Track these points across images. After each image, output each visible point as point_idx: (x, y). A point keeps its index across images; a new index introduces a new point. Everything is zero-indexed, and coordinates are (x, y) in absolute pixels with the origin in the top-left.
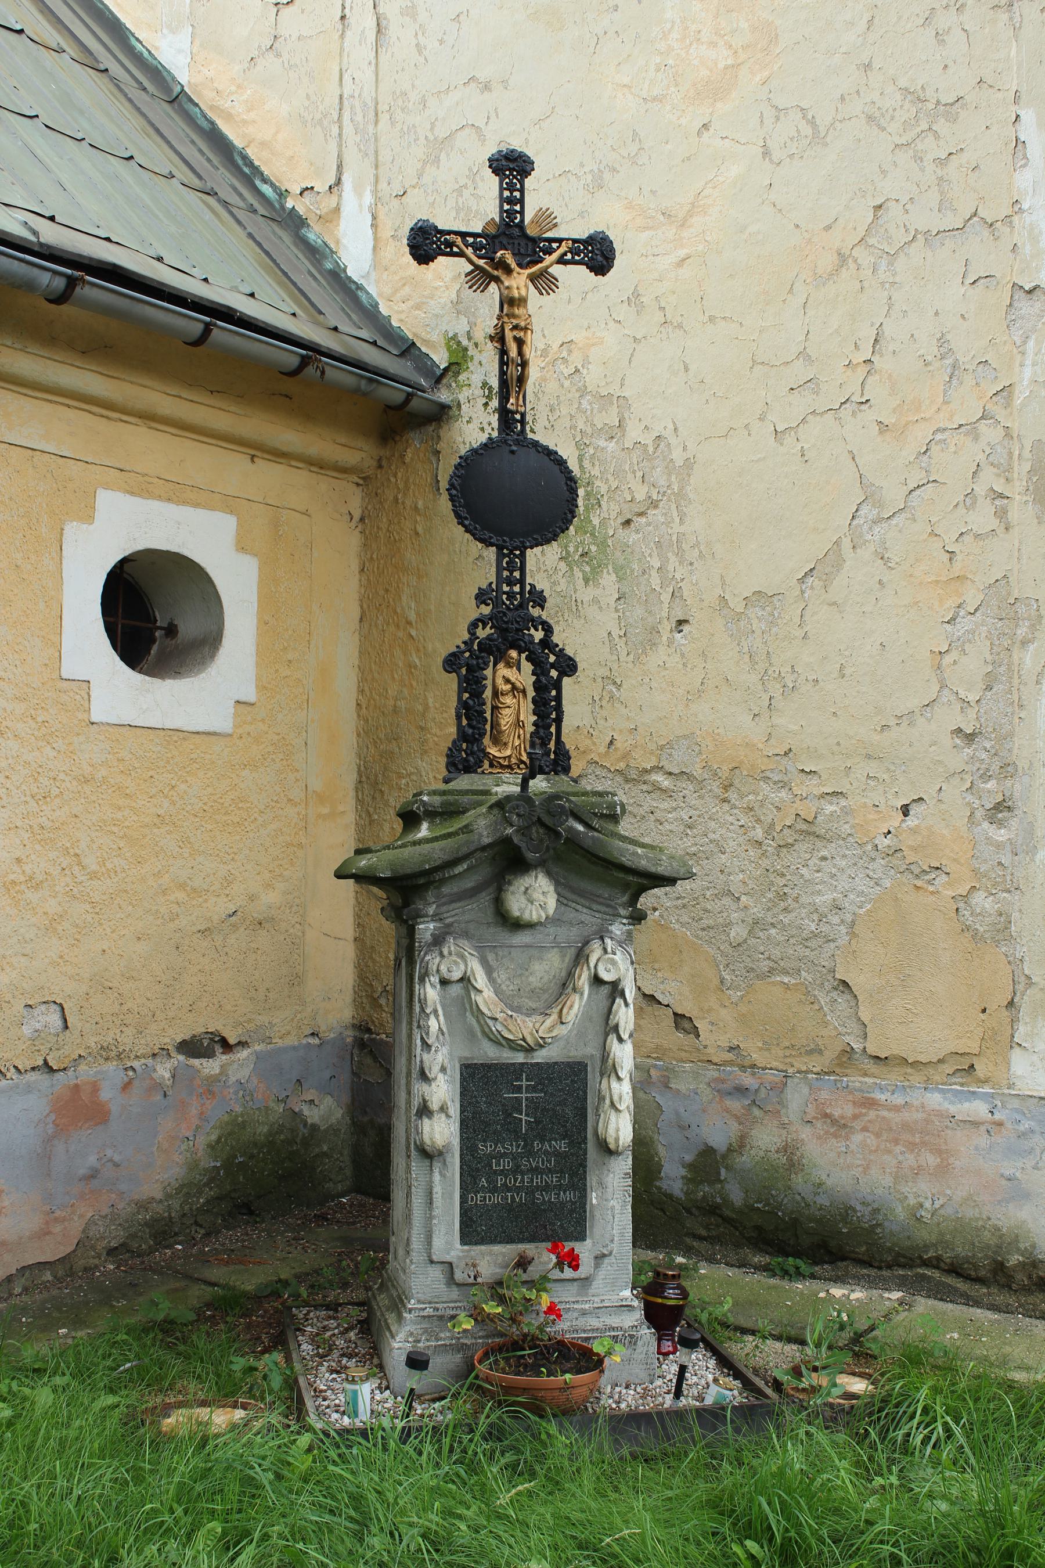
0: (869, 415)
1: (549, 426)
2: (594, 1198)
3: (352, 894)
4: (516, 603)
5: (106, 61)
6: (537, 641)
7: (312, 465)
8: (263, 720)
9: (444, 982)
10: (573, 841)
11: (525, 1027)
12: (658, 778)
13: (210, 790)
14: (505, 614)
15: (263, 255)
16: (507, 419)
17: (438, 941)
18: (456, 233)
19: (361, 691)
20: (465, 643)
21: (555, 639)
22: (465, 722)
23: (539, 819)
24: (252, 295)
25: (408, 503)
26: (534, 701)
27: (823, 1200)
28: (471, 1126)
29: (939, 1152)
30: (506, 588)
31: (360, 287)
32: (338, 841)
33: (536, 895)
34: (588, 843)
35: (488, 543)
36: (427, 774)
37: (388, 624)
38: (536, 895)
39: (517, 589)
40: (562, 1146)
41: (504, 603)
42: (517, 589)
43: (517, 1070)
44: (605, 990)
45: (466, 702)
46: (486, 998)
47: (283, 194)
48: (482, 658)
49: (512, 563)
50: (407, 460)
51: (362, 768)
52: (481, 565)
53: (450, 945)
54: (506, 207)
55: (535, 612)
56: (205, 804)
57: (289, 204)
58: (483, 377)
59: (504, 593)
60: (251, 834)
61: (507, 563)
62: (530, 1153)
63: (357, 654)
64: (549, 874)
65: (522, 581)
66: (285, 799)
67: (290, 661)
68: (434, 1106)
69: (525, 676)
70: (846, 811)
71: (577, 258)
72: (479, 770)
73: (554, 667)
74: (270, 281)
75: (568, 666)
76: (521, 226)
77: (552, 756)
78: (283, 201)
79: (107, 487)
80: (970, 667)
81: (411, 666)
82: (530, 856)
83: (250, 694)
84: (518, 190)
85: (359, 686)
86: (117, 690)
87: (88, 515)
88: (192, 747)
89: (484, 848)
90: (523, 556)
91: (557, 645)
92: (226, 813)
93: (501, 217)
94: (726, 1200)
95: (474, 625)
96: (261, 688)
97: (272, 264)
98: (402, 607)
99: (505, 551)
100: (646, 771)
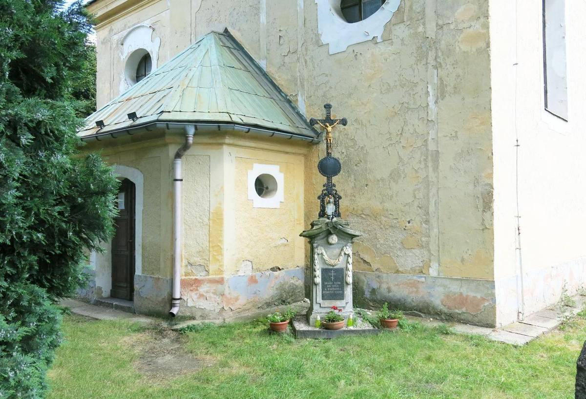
0: (401, 145)
2: (345, 292)
3: (304, 241)
5: (250, 69)
9: (318, 254)
10: (340, 229)
11: (332, 262)
12: (362, 215)
16: (328, 153)
17: (317, 247)
19: (305, 198)
21: (337, 193)
25: (313, 160)
27: (395, 298)
28: (323, 279)
29: (416, 288)
31: (303, 116)
32: (301, 229)
33: (334, 239)
35: (325, 176)
36: (315, 216)
38: (334, 239)
40: (340, 283)
43: (331, 269)
44: (347, 256)
46: (326, 257)
47: (287, 96)
49: (329, 179)
52: (324, 179)
53: (319, 248)
55: (334, 188)
62: (334, 284)
64: (336, 235)
65: (331, 183)
68: (317, 276)
69: (332, 200)
70: (398, 222)
79: (255, 163)
80: (420, 195)
81: (314, 193)
82: (332, 232)
86: (259, 201)
87: (252, 168)
89: (324, 231)
90: (331, 178)
94: (377, 299)
95: (323, 191)
96: (285, 199)
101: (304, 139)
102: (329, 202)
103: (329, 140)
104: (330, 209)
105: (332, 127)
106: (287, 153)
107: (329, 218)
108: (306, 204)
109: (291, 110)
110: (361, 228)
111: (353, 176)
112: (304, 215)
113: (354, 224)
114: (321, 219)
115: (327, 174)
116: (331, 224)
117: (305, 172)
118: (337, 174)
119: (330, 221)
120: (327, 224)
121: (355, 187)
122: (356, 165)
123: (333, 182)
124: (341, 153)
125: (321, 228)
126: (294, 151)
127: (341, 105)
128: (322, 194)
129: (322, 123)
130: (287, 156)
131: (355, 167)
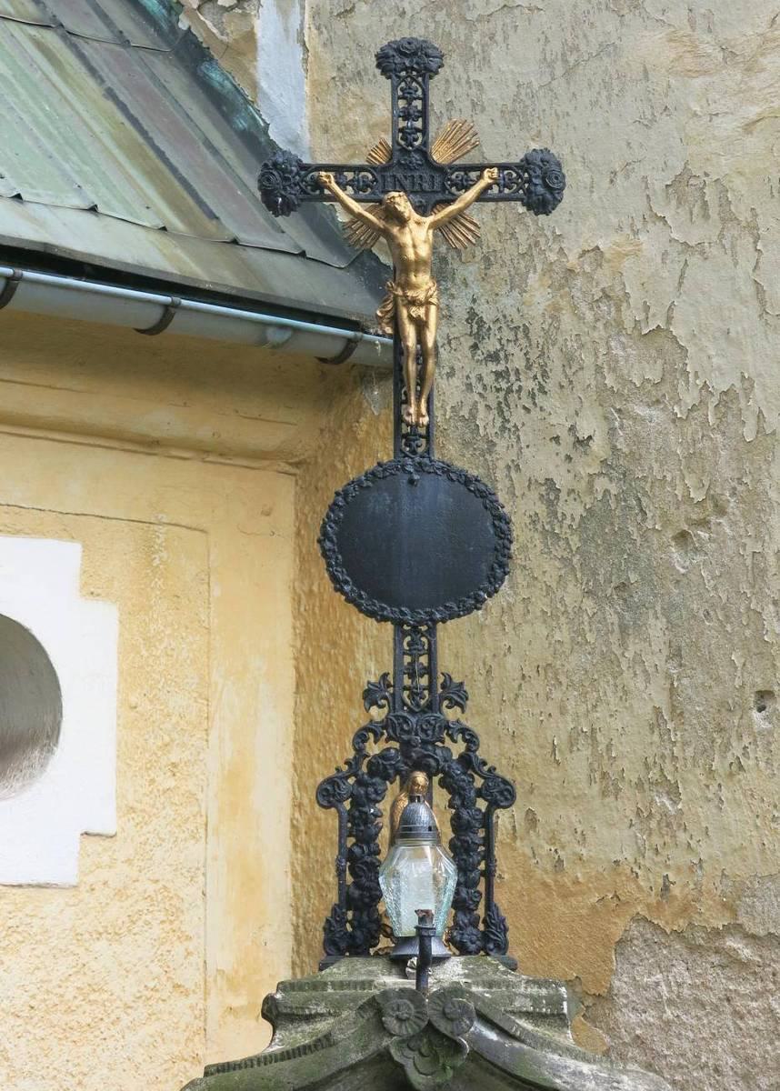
1: (565, 383)
4: (422, 702)
6: (455, 757)
7: (207, 452)
8: (129, 861)
12: (732, 943)
13: (40, 974)
14: (406, 720)
15: (128, 125)
18: (327, 168)
20: (347, 763)
21: (481, 754)
22: (349, 879)
23: (430, 1024)
24: (93, 209)
26: (452, 846)
30: (407, 681)
34: (504, 1059)
35: (384, 619)
37: (336, 696)
39: (424, 681)
41: (405, 704)
42: (424, 681)
45: (350, 851)
48: (374, 784)
50: (361, 435)
51: (301, 930)
54: (402, 124)
55: (451, 714)
56: (33, 997)
57: (183, 24)
58: (469, 304)
59: (405, 688)
60: (111, 1043)
61: (409, 644)
63: (290, 746)
65: (430, 670)
66: (169, 985)
67: (174, 765)
69: (433, 812)
71: (506, 191)
72: (372, 951)
73: (478, 798)
74: (134, 172)
75: (501, 793)
76: (424, 153)
77: (481, 927)
78: (174, 19)
83: (106, 821)
84: (419, 98)
85: (295, 798)
88: (10, 908)
89: (353, 1068)
90: (432, 632)
91: (484, 763)
92: (69, 1011)
93: (395, 141)
95: (361, 737)
97: (141, 140)
98: (357, 670)
99: (405, 627)
100: (717, 933)
101: (275, 336)
102: (405, 831)
103: (410, 331)
104: (417, 884)
105: (435, 226)
106: (150, 445)
107: (398, 963)
108: (306, 853)
109: (194, 107)
110: (721, 1045)
111: (656, 628)
112: (290, 943)
113: (669, 1014)
114: (340, 971)
115: (394, 602)
116: (408, 1009)
117: (297, 600)
118: (478, 603)
119: (411, 984)
120: (376, 1008)
121: (677, 713)
122: (682, 537)
123: (448, 663)
124: (567, 439)
125: (325, 1041)
126: (204, 432)
127: (569, 72)
128: (353, 765)
129: (359, 188)
130: (143, 468)
131: (675, 553)
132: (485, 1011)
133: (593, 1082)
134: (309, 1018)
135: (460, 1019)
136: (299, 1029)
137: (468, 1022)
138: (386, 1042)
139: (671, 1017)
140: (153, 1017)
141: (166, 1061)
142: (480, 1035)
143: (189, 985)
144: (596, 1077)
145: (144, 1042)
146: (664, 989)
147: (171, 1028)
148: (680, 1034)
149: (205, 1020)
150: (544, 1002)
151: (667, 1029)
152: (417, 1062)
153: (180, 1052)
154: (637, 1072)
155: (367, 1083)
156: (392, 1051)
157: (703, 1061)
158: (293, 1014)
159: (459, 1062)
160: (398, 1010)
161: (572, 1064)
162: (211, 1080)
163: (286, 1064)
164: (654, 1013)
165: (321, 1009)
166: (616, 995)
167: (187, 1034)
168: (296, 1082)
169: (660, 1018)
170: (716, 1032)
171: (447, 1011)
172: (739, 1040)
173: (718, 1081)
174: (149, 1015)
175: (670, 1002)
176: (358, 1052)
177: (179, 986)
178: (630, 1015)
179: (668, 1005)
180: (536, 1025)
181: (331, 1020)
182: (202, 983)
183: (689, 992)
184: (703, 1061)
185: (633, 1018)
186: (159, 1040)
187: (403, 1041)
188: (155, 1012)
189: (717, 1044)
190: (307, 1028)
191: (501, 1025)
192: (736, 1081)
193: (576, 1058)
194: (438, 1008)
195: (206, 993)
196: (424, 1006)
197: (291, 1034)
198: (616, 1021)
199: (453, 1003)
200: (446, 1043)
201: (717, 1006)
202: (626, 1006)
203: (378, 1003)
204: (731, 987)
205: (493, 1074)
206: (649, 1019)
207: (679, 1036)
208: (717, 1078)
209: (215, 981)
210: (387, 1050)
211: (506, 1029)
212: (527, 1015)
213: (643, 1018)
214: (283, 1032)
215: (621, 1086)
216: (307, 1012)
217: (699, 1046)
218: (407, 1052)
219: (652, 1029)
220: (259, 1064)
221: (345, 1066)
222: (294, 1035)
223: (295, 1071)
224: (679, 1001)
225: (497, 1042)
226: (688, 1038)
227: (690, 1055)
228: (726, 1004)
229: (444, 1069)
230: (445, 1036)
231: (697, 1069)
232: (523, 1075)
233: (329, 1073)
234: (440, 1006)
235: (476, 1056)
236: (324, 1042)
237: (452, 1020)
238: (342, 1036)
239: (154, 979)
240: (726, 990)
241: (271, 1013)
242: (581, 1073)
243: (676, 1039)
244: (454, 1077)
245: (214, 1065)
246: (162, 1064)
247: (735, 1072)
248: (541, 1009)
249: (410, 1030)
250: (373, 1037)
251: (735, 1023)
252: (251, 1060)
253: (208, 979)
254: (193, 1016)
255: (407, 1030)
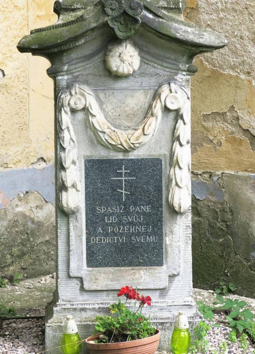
34: (155, 25)
66: (12, 6)
89: (93, 30)
113: (222, 15)
125: (81, 19)
132: (148, 6)
133: (192, 35)
134: (74, 10)
135: (137, 9)
136: (70, 15)
137: (140, 10)
138: (106, 19)
139: (223, 16)
140: (6, 19)
141: (12, 37)
142: (145, 16)
143: (21, 6)
144: (193, 33)
145: (2, 29)
146: (219, 4)
147: (14, 24)
148: (226, 23)
149: (28, 21)
150: (172, 3)
151: (221, 21)
152: (119, 27)
153: (17, 33)
154: (210, 31)
155: (98, 37)
156: (109, 22)
157: (236, 34)
158: (67, 8)
159: (137, 27)
160: (111, 5)
161: (184, 28)
162: (33, 35)
163: (65, 28)
164: (215, 15)
165: (79, 6)
166: (199, 8)
167: (21, 26)
168: (69, 35)
169: (218, 17)
170: (241, 22)
171: (131, 5)
172: (251, 25)
173: (242, 42)
174: (4, 18)
175: (222, 10)
176: (94, 23)
177: (17, 6)
178: (206, 16)
179: (221, 11)
180: (169, 13)
181: (83, 11)
182: (26, 5)
183: (230, 6)
184: (236, 34)
185: (207, 17)
186: (9, 29)
187: (113, 18)
188: (7, 17)
189: (242, 27)
190: (73, 14)
191: (154, 11)
192: (249, 42)
193: (185, 25)
194: (128, 5)
195: (28, 9)
196: (122, 3)
197: (66, 17)
198: (199, 18)
199: (134, 2)
200: (131, 19)
201: (242, 11)
202: (204, 12)
203: (103, 3)
204: (248, 3)
205: (150, 32)
206: (213, 17)
207: (226, 24)
208: (242, 41)
209: (32, 4)
210: (107, 22)
211: (156, 13)
212: (165, 8)
213: (211, 17)
214: (63, 16)
215: (204, 37)
216: (73, 7)
217: (234, 28)
218: (115, 23)
219: (214, 21)
220: (53, 29)
221: (89, 29)
222: (67, 17)
223: (68, 31)
224: (226, 9)
225: (153, 19)
226: (229, 25)
227: (230, 32)
228: (245, 10)
229: (130, 29)
230: (131, 16)
231: (233, 37)
232: (154, 153)
233: (82, 32)
234: (129, 4)
235: (144, 25)
236: (80, 19)
237: (134, 9)
238: (88, 17)
239: (6, 3)
240: (245, 4)
241: (58, 8)
242: (187, 31)
243: (225, 26)
244: (134, 34)
245: (34, 30)
246: (10, 39)
247: (249, 38)
248: (170, 6)
249: (116, 14)
250: (101, 17)
251: (249, 18)
252: (50, 27)
253: (28, 4)
254: (23, 19)
255: (115, 14)
